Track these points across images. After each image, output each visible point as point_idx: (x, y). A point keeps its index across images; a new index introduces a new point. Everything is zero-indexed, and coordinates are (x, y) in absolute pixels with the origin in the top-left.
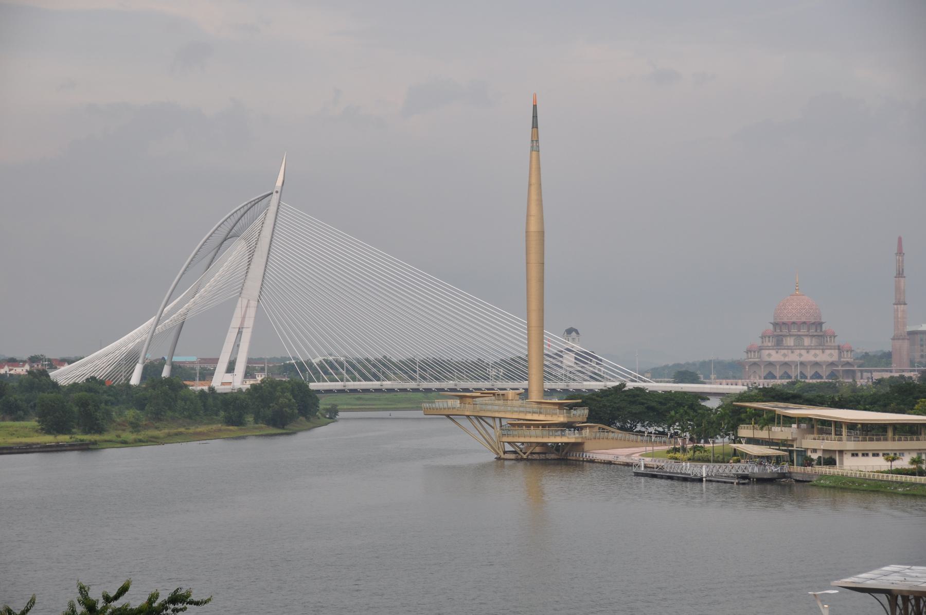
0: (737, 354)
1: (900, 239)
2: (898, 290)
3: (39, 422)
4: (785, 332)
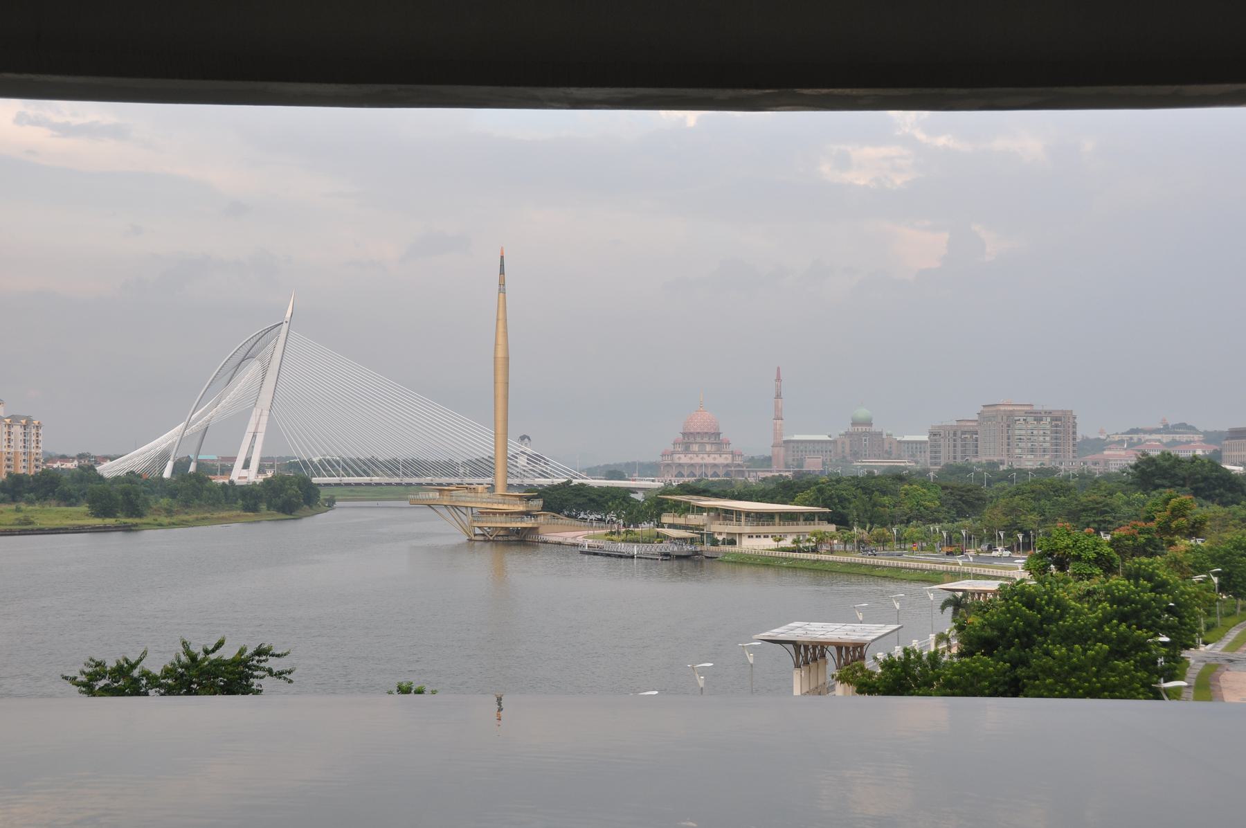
1: (778, 368)
2: (777, 409)
3: (89, 507)
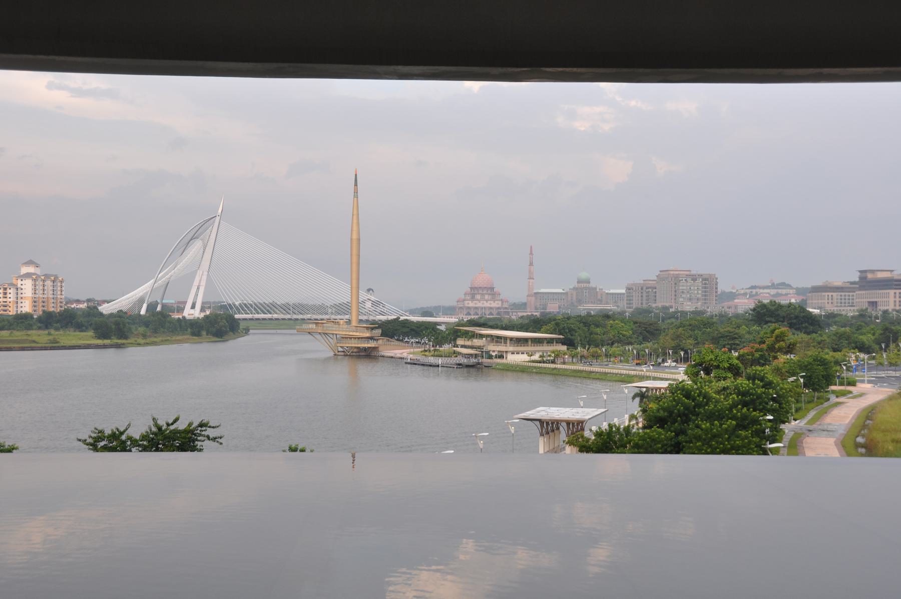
0: (452, 303)
1: (531, 247)
4: (476, 292)
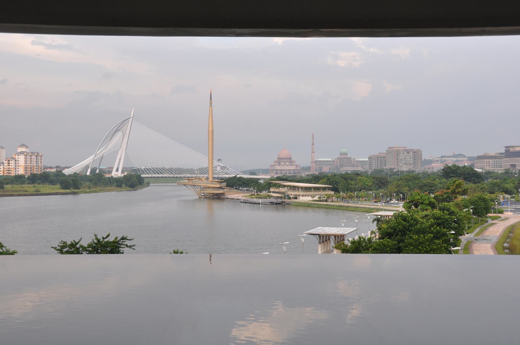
0: (267, 167)
1: (313, 134)
2: (312, 148)
4: (281, 160)
